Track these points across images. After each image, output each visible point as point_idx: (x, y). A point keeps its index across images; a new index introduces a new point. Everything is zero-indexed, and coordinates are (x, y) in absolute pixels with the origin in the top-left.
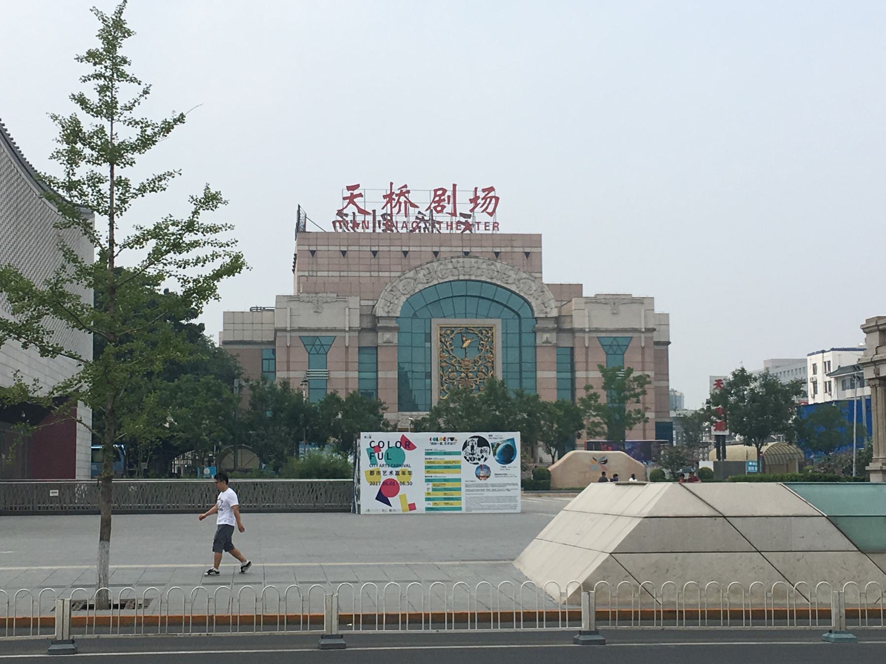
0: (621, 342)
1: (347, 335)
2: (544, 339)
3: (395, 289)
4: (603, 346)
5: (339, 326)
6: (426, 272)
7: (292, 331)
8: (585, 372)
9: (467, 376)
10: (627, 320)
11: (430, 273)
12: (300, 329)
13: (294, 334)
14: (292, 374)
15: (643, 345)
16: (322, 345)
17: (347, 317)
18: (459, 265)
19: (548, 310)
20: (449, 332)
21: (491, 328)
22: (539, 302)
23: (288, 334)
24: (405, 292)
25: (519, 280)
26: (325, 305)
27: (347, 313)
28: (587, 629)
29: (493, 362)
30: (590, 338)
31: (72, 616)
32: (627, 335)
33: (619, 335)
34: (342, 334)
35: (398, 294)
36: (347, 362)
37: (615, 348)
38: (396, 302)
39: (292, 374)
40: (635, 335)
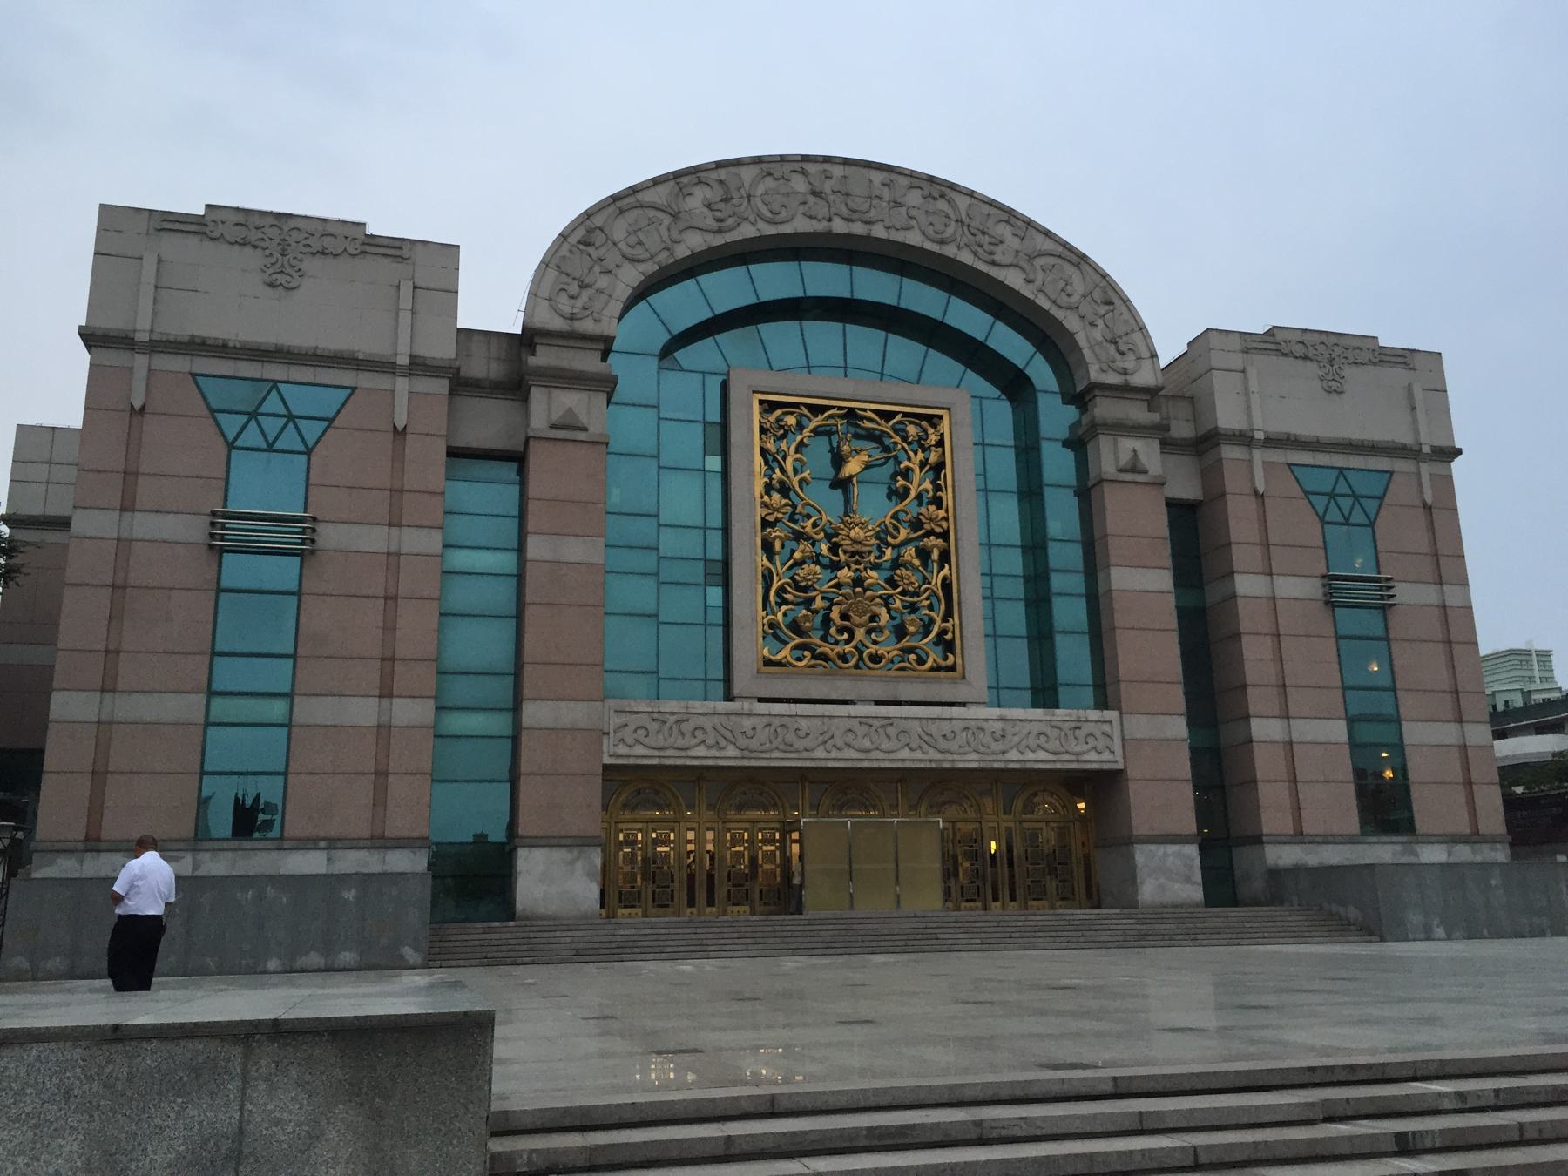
0: (1361, 485)
1: (402, 384)
2: (1125, 458)
3: (599, 238)
4: (1307, 493)
5: (367, 344)
6: (714, 194)
7: (158, 346)
8: (1263, 579)
9: (858, 582)
10: (1365, 414)
11: (726, 200)
12: (196, 346)
13: (164, 362)
14: (143, 526)
15: (329, 536)
16: (291, 418)
17: (405, 317)
18: (827, 187)
19: (1129, 362)
20: (791, 420)
21: (934, 420)
22: (1097, 334)
23: (141, 361)
24: (638, 252)
25: (1030, 258)
26: (310, 265)
27: (406, 303)
28: (719, 459)
29: (945, 535)
30: (1268, 466)
31: (228, 832)
32: (1383, 463)
33: (1356, 461)
34: (381, 381)
35: (612, 258)
36: (397, 492)
37: (1346, 503)
38: (603, 282)
39: (143, 526)
40: (1400, 466)
